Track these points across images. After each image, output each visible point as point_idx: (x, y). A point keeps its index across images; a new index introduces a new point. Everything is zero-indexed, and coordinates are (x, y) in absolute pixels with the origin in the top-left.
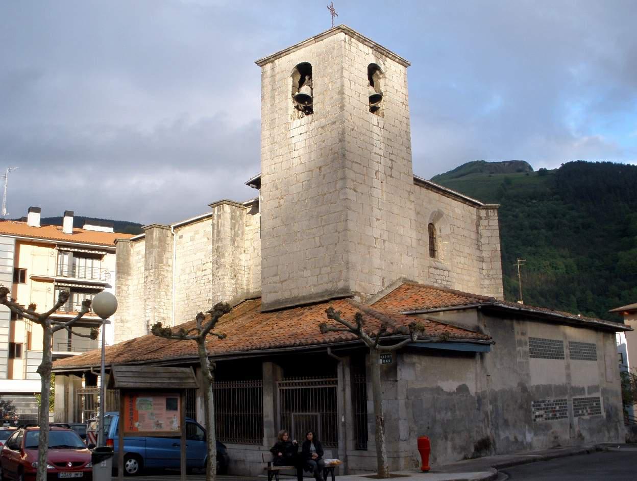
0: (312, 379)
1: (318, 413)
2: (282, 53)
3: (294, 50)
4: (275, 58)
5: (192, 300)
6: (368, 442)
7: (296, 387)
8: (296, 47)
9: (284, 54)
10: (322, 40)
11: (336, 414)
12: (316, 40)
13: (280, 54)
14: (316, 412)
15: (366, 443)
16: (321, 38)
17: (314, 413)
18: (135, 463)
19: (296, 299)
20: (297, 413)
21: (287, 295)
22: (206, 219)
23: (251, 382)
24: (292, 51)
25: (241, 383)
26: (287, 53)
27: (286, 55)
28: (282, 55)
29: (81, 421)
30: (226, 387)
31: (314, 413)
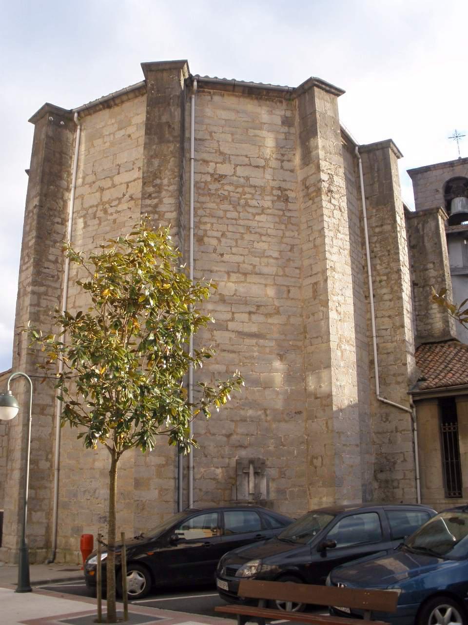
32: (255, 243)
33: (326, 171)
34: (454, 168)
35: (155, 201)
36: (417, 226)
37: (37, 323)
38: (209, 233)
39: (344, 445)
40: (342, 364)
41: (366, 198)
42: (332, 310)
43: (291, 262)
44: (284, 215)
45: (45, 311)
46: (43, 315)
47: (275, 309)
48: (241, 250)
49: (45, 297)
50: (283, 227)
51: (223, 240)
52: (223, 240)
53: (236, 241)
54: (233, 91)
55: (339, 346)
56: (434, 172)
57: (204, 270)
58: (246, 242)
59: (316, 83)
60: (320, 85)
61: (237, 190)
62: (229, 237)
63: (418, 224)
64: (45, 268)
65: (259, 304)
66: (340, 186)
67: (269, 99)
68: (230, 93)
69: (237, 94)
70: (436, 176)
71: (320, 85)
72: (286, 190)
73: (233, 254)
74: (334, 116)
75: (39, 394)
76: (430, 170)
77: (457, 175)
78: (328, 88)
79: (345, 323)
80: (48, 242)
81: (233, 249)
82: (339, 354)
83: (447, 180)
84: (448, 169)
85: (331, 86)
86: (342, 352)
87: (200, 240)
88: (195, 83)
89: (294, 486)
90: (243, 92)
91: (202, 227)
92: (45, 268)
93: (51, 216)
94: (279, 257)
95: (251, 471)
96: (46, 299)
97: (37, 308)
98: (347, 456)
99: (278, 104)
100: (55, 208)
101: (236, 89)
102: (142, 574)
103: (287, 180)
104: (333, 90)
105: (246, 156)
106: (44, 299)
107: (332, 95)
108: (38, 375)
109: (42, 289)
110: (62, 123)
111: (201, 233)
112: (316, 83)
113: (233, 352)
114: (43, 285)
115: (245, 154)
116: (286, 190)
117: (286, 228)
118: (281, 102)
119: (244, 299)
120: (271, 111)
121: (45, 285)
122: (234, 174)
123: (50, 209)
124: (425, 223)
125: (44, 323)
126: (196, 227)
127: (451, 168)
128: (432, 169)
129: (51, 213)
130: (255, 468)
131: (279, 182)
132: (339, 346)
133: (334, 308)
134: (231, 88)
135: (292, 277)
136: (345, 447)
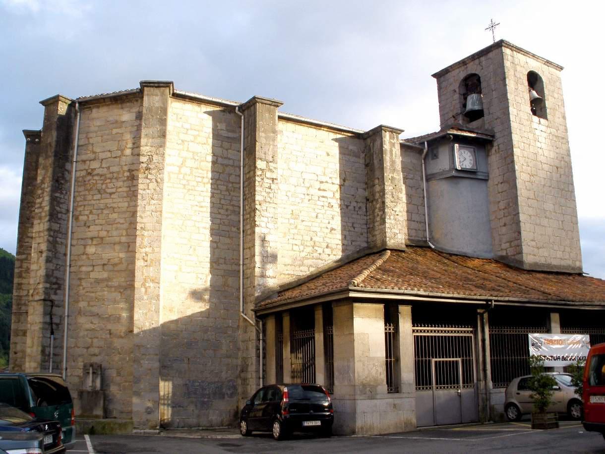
0: (465, 327)
1: (459, 360)
2: (523, 52)
3: (531, 56)
4: (516, 50)
5: (303, 221)
6: (334, 387)
7: (438, 335)
8: (534, 56)
9: (523, 53)
10: (548, 66)
11: (415, 358)
12: (546, 63)
13: (522, 51)
14: (456, 357)
15: (333, 387)
16: (548, 64)
17: (455, 359)
18: (573, 407)
19: (549, 265)
20: (438, 359)
21: (543, 261)
22: (325, 129)
23: (516, 328)
24: (529, 55)
25: (311, 331)
26: (525, 54)
27: (524, 55)
28: (521, 52)
29: (28, 402)
30: (301, 337)
31: (455, 359)
32: (110, 215)
33: (146, 154)
34: (467, 65)
35: (41, 199)
36: (369, 146)
37: (20, 279)
38: (82, 213)
39: (143, 355)
40: (145, 297)
41: (244, 149)
42: (138, 259)
43: (132, 225)
44: (130, 190)
45: (26, 270)
46: (25, 273)
47: (120, 260)
48: (100, 221)
49: (26, 261)
50: (128, 199)
51: (90, 216)
52: (90, 216)
53: (98, 215)
54: (104, 102)
55: (143, 285)
56: (453, 72)
57: (78, 239)
58: (104, 215)
59: (144, 84)
60: (149, 85)
61: (102, 178)
62: (94, 213)
63: (370, 143)
64: (26, 242)
65: (110, 258)
66: (160, 162)
67: (130, 101)
68: (102, 104)
69: (107, 103)
70: (454, 76)
71: (149, 85)
72: (133, 171)
73: (96, 225)
74: (162, 106)
75: (22, 323)
76: (450, 72)
77: (469, 72)
78: (156, 85)
79: (151, 268)
80: (27, 225)
81: (96, 221)
82: (143, 290)
83: (462, 78)
84: (463, 67)
85: (159, 83)
86: (146, 289)
87: (76, 218)
88: (77, 105)
89: (126, 381)
90: (111, 101)
91: (79, 209)
92: (26, 242)
93: (29, 207)
94: (124, 222)
95: (91, 371)
96: (27, 263)
97: (20, 269)
98: (146, 362)
99: (135, 103)
100: (32, 201)
101: (106, 100)
102: (304, 402)
103: (135, 162)
104: (161, 85)
105: (109, 151)
106: (25, 263)
107: (162, 88)
108: (21, 311)
109: (24, 257)
110: (37, 140)
111: (77, 213)
112: (144, 84)
113: (93, 292)
114: (24, 254)
115: (109, 149)
116: (133, 171)
117: (131, 200)
118: (137, 101)
119: (100, 255)
120: (130, 111)
121: (26, 254)
122: (101, 167)
123: (28, 203)
124: (374, 141)
125: (25, 278)
126: (75, 209)
127: (465, 66)
128: (451, 70)
129: (29, 205)
130: (93, 369)
131: (130, 166)
132: (143, 285)
133: (140, 258)
134: (102, 101)
135: (132, 236)
136: (144, 356)
